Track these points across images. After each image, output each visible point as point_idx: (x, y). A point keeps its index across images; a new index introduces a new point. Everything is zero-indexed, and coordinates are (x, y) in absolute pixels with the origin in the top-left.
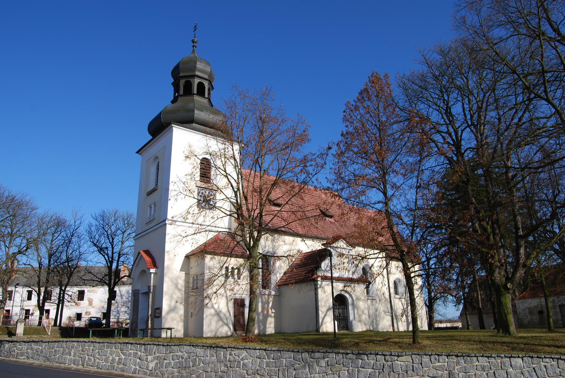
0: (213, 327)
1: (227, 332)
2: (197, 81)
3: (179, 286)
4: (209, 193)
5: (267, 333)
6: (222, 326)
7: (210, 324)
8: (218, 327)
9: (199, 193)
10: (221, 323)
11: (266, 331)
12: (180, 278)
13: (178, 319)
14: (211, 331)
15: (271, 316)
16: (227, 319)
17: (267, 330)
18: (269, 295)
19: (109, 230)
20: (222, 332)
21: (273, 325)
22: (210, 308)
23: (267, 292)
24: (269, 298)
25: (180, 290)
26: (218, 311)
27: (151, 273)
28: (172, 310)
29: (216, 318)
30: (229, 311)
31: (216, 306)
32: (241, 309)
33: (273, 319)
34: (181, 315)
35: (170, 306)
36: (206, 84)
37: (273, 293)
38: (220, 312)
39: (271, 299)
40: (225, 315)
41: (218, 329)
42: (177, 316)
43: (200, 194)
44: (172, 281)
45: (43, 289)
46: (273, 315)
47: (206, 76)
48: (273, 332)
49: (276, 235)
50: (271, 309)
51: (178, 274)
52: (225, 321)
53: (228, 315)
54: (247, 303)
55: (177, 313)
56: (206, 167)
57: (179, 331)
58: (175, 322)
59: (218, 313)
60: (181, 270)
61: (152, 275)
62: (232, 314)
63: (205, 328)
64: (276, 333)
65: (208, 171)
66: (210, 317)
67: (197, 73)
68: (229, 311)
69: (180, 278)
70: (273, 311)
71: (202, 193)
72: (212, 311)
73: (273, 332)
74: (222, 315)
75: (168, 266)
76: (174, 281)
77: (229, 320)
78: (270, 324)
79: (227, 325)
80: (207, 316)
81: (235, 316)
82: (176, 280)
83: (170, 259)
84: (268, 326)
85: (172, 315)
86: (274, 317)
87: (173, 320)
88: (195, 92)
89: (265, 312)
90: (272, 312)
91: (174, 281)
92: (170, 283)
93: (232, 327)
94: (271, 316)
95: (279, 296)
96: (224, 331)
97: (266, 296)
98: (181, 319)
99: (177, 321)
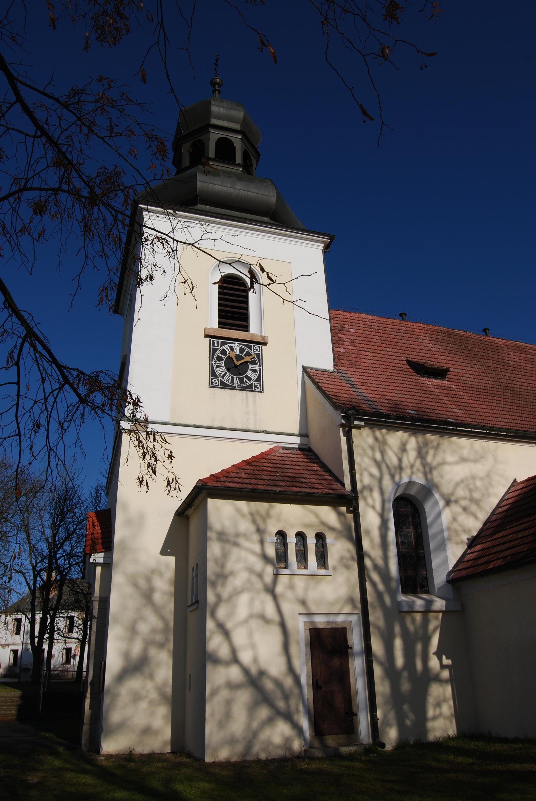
0: (238, 724)
1: (288, 741)
2: (214, 136)
3: (157, 597)
4: (242, 350)
5: (432, 737)
6: (270, 721)
7: (228, 715)
8: (255, 725)
9: (214, 350)
10: (264, 712)
11: (425, 731)
12: (161, 574)
13: (154, 695)
14: (232, 741)
15: (437, 679)
16: (286, 697)
17: (430, 724)
18: (427, 611)
19: (70, 483)
20: (269, 742)
21: (447, 709)
22: (227, 664)
23: (419, 603)
24: (426, 622)
25: (157, 610)
26: (254, 671)
27: (96, 565)
28: (136, 667)
29: (244, 697)
30: (291, 670)
31: (246, 657)
32: (336, 662)
33: (448, 690)
34: (165, 685)
35: (126, 655)
36: (236, 139)
37: (439, 604)
38: (262, 673)
39: (434, 623)
40: (278, 683)
41: (255, 734)
42: (150, 685)
43: (218, 353)
44: (136, 585)
45: (38, 616)
46: (446, 674)
47: (237, 127)
48: (452, 731)
49: (431, 437)
50: (439, 654)
51: (152, 563)
52: (281, 704)
53: (289, 682)
54: (356, 641)
55: (151, 677)
56: (234, 299)
57: (156, 733)
58: (143, 705)
59: (254, 680)
60: (164, 552)
61: (99, 569)
62: (304, 679)
63: (210, 728)
64: (462, 735)
65: (222, 290)
66: (224, 694)
67: (214, 121)
68: (291, 670)
69: (161, 574)
70: (446, 661)
71: (224, 352)
72: (234, 673)
73: (452, 731)
74: (269, 685)
75: (122, 542)
76: (142, 583)
77: (293, 702)
78: (438, 705)
79: (288, 717)
80: (215, 692)
81: (316, 686)
82: (149, 580)
83: (129, 522)
84: (431, 713)
85: (134, 684)
86: (452, 680)
87: (137, 698)
88: (212, 153)
89: (419, 665)
90: (443, 667)
91: (142, 583)
92: (129, 590)
93: (305, 723)
94: (437, 679)
95: (457, 618)
96: (277, 740)
97: (418, 617)
98: (163, 696)
99: (151, 702)
